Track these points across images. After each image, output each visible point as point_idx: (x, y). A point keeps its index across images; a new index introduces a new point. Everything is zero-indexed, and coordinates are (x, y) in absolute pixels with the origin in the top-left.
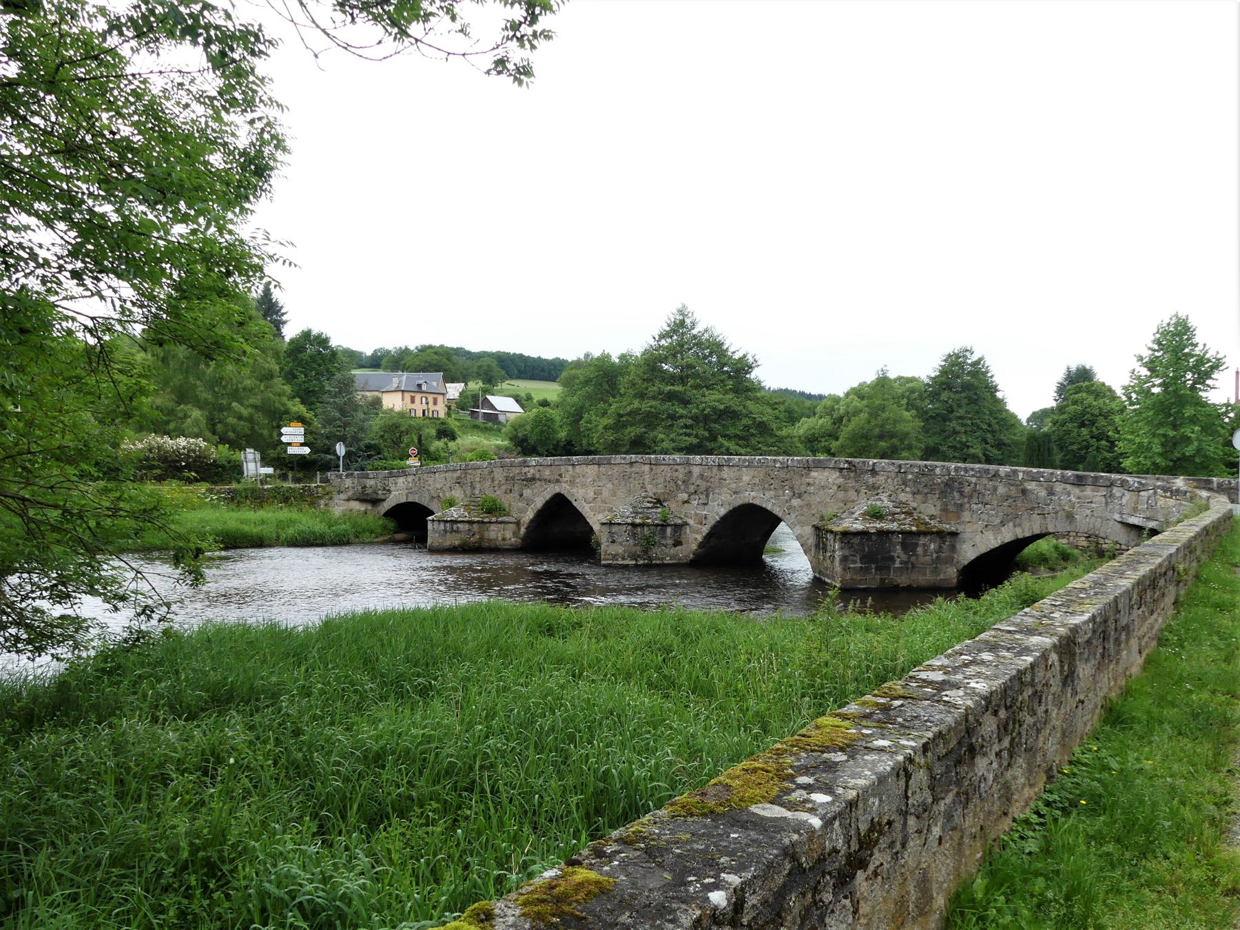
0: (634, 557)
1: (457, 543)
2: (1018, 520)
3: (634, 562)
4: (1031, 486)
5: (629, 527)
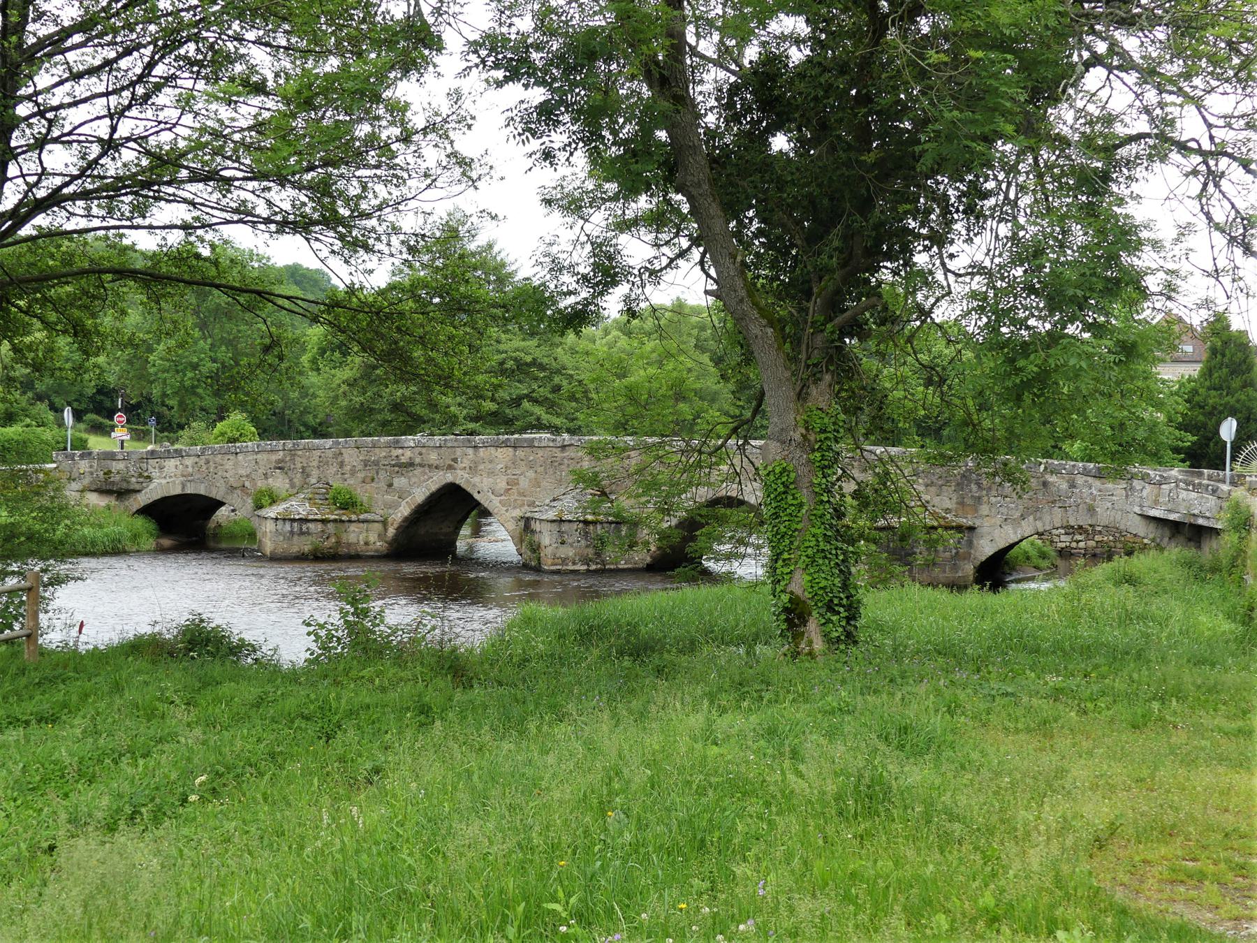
0: (587, 561)
1: (307, 549)
2: (1038, 514)
3: (585, 567)
4: (1052, 479)
5: (581, 525)
